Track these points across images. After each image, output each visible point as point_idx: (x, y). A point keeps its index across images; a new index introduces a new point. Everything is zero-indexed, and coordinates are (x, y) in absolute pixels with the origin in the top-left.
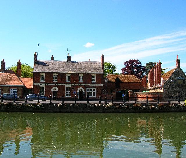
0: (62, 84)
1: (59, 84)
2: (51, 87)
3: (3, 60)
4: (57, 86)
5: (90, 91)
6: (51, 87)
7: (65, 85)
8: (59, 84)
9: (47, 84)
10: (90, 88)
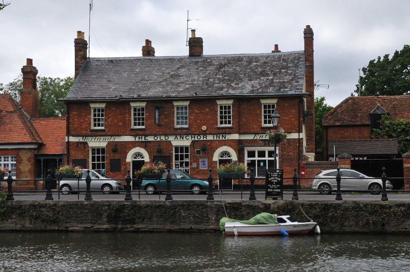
0: (163, 138)
1: (150, 139)
3: (30, 61)
4: (145, 145)
5: (257, 158)
7: (171, 138)
8: (150, 139)
9: (112, 139)
10: (257, 149)
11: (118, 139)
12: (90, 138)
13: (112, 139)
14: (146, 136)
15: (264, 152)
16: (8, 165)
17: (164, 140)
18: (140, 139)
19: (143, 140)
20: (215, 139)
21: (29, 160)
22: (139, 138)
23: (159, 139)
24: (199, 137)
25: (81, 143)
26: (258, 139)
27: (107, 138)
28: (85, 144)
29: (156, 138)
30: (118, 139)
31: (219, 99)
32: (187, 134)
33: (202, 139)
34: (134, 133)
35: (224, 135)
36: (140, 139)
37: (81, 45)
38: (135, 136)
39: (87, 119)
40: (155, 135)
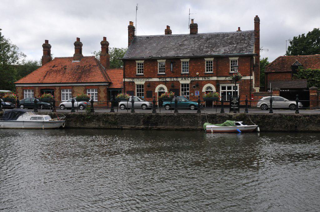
0: (175, 79)
1: (168, 80)
2: (156, 84)
4: (165, 83)
6: (156, 84)
7: (179, 79)
8: (168, 80)
9: (147, 80)
10: (226, 85)
11: (151, 80)
13: (147, 80)
14: (166, 78)
17: (176, 80)
19: (164, 80)
20: (204, 80)
21: (104, 91)
23: (172, 80)
24: (195, 79)
25: (131, 82)
26: (228, 79)
27: (145, 79)
28: (133, 82)
29: (171, 79)
30: (151, 80)
31: (206, 58)
32: (188, 77)
33: (196, 80)
34: (159, 76)
35: (208, 77)
37: (131, 29)
38: (160, 78)
39: (134, 69)
40: (171, 78)
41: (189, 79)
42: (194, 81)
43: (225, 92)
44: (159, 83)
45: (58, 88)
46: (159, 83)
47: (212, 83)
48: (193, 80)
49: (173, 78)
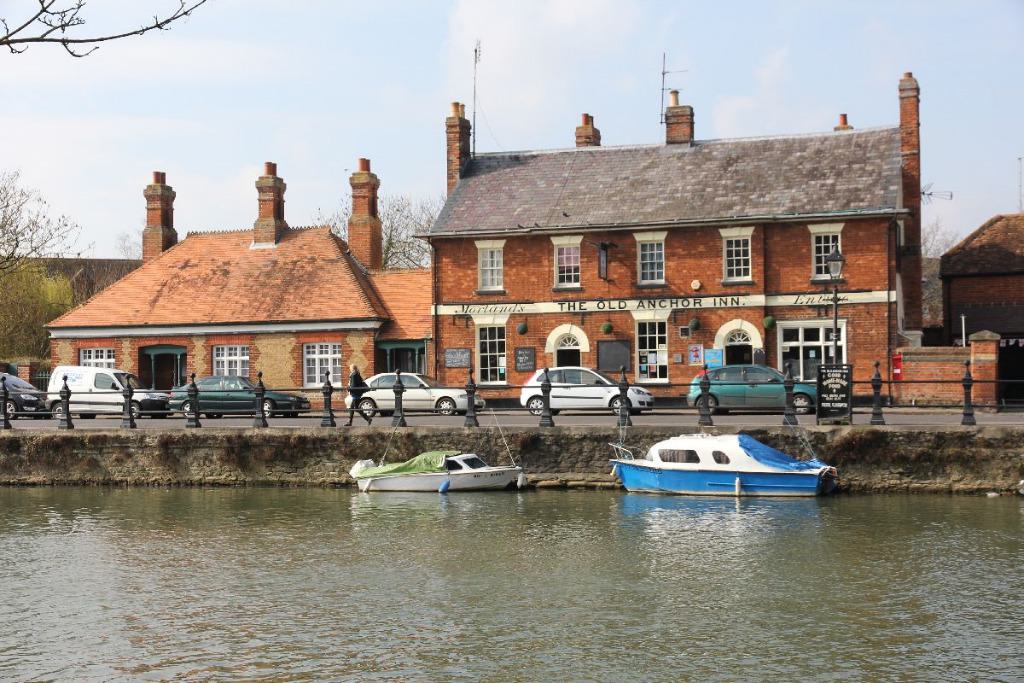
0: (615, 304)
1: (591, 306)
5: (801, 343)
7: (632, 305)
8: (591, 306)
11: (528, 308)
12: (477, 307)
15: (816, 331)
16: (327, 360)
18: (572, 309)
21: (364, 352)
22: (672, 303)
25: (460, 316)
28: (468, 318)
30: (528, 308)
36: (572, 309)
41: (667, 303)
42: (682, 311)
43: (797, 348)
44: (558, 319)
45: (199, 344)
46: (558, 319)
47: (582, 324)
48: (680, 306)
49: (609, 300)
